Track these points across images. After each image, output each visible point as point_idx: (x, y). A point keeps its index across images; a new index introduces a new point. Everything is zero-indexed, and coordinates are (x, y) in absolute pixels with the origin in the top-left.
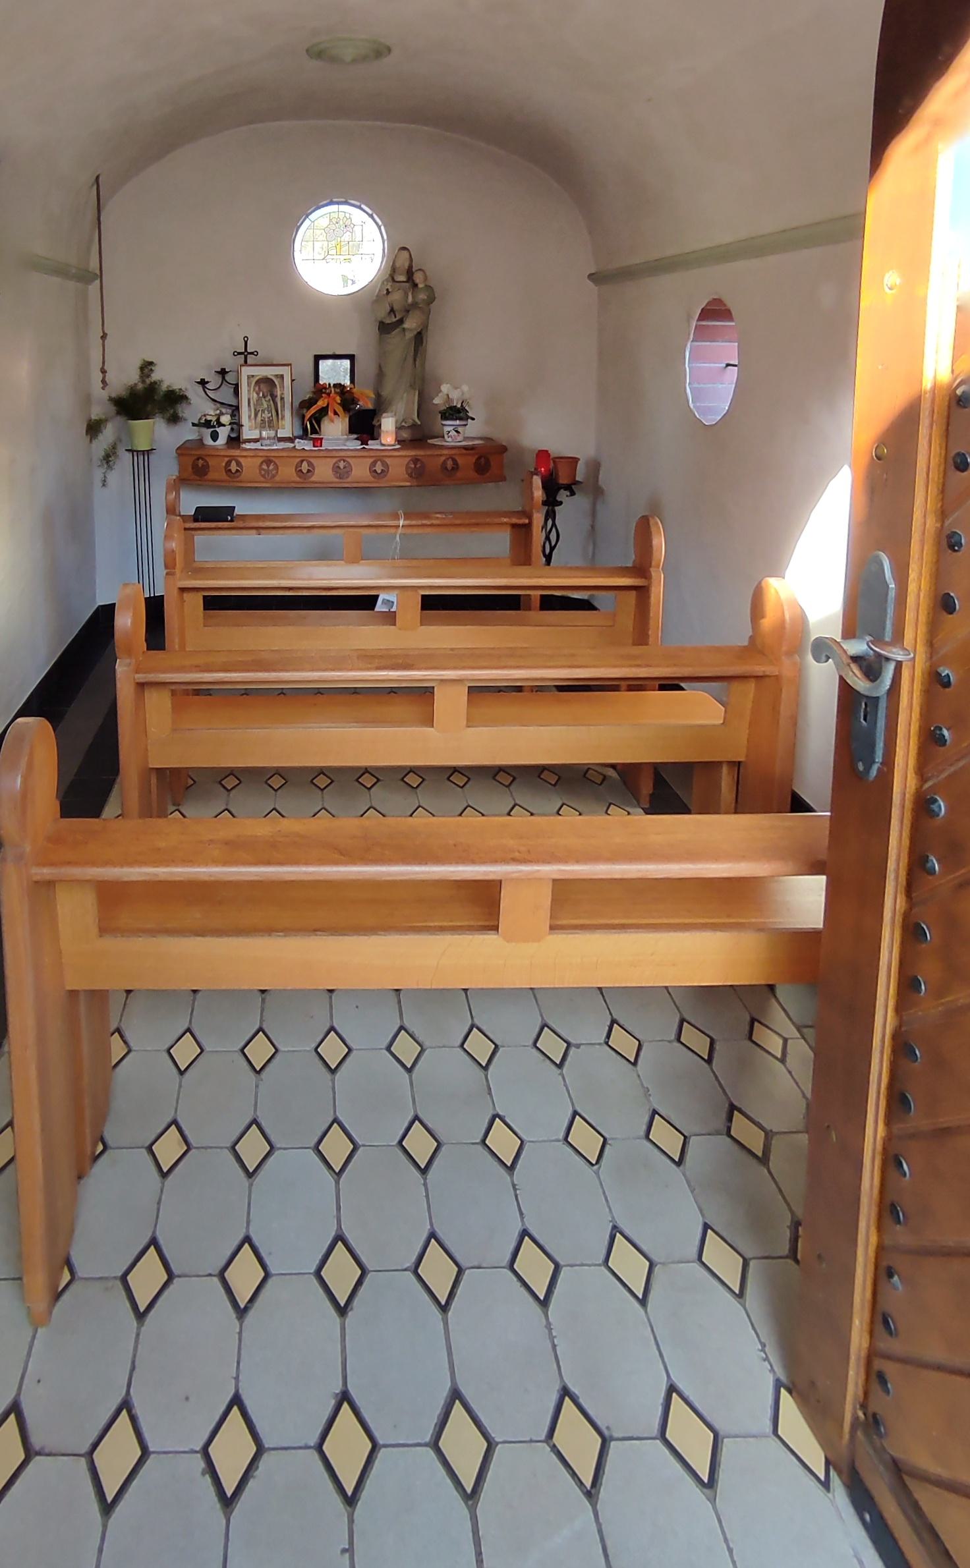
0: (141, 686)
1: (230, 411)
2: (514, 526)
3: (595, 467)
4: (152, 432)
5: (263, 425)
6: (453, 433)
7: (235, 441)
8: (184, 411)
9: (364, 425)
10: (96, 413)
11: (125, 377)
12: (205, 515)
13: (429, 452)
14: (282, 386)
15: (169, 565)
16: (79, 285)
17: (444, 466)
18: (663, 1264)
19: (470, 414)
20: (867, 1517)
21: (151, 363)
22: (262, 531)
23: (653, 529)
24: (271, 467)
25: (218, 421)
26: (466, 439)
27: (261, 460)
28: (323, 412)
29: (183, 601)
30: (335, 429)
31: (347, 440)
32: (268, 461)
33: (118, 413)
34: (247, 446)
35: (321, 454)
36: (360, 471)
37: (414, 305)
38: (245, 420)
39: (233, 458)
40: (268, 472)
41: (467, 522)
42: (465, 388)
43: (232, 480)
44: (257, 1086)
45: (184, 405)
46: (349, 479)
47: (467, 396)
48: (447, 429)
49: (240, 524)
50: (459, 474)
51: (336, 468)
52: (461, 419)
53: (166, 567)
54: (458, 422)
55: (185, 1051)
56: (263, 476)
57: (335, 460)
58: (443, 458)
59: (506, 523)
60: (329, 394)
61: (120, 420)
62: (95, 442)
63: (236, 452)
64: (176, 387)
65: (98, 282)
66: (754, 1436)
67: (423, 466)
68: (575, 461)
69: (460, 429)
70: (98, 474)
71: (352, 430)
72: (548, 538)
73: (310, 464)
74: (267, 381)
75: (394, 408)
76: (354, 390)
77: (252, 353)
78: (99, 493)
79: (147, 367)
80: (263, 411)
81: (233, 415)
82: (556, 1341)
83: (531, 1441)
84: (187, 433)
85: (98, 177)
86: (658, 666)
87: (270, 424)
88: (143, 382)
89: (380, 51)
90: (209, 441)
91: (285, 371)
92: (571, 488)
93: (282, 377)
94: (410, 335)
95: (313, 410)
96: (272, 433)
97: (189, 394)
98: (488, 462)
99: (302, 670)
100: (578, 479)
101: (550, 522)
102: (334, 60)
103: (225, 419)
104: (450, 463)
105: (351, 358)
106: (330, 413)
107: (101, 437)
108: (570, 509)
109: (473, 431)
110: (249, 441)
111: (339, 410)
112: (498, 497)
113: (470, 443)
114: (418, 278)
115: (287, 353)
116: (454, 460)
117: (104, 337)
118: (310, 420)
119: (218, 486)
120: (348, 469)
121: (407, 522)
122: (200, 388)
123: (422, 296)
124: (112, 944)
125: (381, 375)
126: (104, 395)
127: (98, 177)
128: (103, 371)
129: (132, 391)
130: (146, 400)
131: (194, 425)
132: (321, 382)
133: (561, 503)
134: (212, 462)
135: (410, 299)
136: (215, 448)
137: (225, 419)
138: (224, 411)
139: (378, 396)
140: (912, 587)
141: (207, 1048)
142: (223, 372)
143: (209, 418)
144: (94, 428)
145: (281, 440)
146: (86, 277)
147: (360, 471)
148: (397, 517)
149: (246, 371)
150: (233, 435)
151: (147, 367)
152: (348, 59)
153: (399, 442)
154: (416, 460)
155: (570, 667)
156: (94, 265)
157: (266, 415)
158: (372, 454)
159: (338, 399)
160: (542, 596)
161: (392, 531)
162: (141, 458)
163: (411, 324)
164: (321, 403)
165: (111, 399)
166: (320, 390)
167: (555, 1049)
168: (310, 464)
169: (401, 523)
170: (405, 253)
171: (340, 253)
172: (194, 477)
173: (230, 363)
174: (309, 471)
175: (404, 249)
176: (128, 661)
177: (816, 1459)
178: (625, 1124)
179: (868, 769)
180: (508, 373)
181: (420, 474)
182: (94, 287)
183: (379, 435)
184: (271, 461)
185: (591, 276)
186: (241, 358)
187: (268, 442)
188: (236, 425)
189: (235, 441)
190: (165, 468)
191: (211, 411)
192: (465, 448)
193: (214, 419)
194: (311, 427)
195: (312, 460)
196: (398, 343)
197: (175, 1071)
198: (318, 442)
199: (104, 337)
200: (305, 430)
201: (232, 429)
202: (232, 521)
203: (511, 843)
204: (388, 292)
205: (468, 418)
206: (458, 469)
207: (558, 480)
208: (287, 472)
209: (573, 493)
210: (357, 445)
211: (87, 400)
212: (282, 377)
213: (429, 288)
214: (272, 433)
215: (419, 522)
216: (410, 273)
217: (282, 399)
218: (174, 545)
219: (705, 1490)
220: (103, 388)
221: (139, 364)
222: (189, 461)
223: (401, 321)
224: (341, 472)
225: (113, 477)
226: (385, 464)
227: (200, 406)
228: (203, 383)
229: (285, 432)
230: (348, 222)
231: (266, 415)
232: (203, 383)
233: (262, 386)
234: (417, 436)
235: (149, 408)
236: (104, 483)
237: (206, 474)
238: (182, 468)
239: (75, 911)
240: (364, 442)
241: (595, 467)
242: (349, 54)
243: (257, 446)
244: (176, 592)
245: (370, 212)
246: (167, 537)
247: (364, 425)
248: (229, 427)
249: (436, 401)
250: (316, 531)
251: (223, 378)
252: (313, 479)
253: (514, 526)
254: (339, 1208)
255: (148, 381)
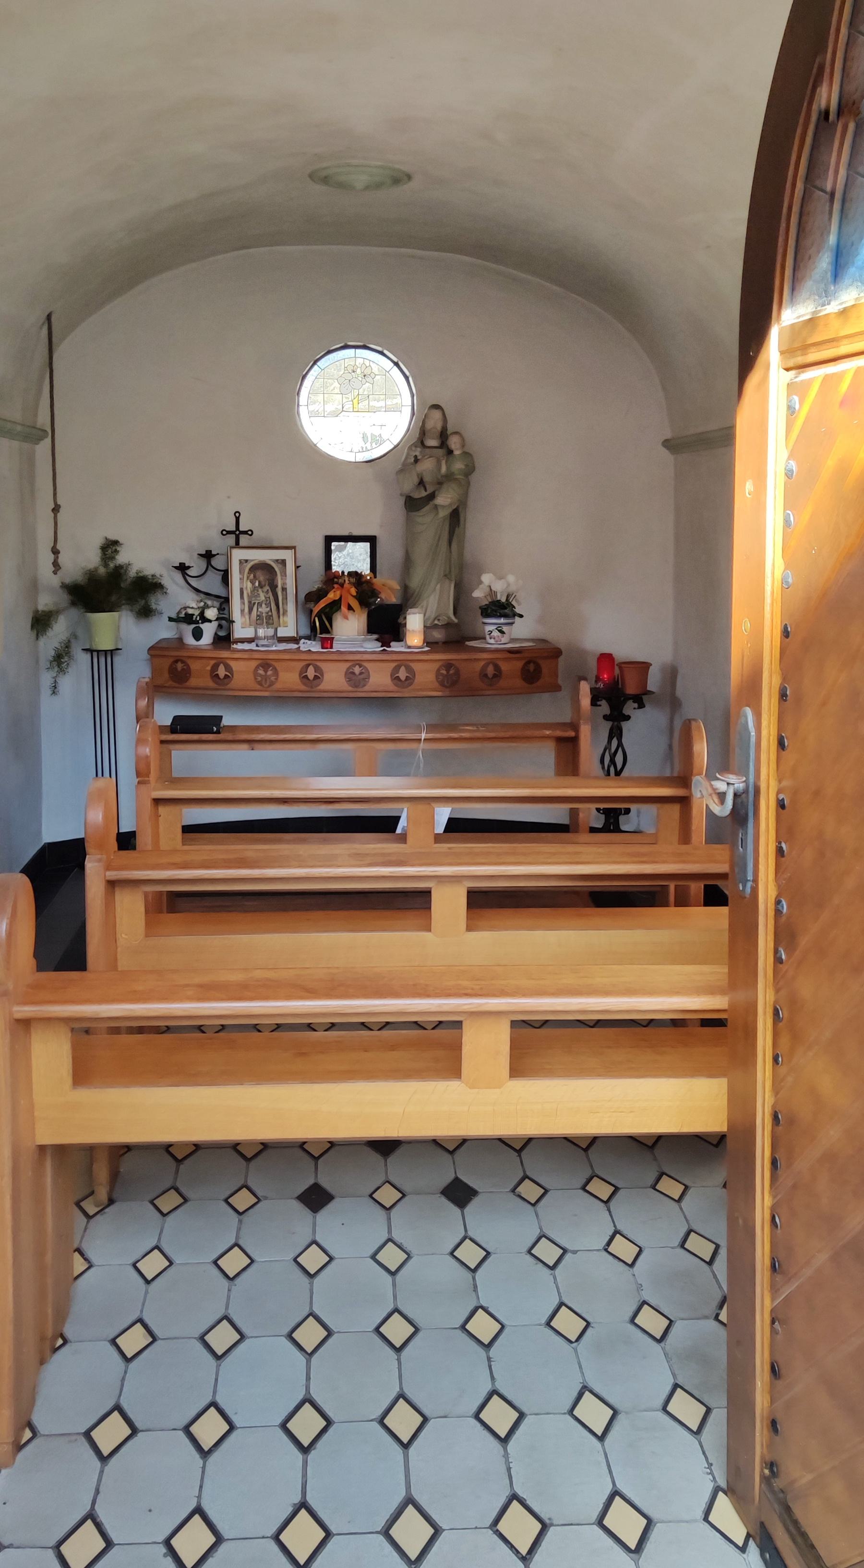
0: (112, 884)
1: (217, 604)
2: (559, 740)
3: (672, 674)
4: (112, 627)
5: (260, 621)
6: (496, 633)
7: (224, 640)
8: (158, 602)
9: (386, 624)
10: (45, 602)
11: (82, 558)
12: (183, 726)
13: (464, 656)
14: (284, 574)
15: (142, 774)
16: (26, 446)
17: (484, 675)
18: (627, 1413)
19: (518, 610)
20: (768, 1556)
21: (116, 543)
22: (256, 745)
23: (695, 733)
24: (270, 673)
25: (202, 614)
26: (513, 640)
27: (254, 664)
28: (335, 606)
29: (158, 816)
30: (350, 628)
31: (364, 640)
32: (265, 665)
33: (73, 604)
34: (240, 646)
35: (335, 657)
36: (379, 679)
37: (449, 477)
38: (236, 615)
39: (219, 661)
40: (266, 678)
41: (502, 734)
42: (511, 578)
43: (220, 685)
44: (229, 1290)
45: (159, 595)
46: (366, 688)
47: (513, 588)
48: (488, 628)
49: (230, 737)
50: (502, 683)
51: (349, 674)
52: (505, 616)
53: (138, 774)
54: (502, 620)
55: (152, 1265)
56: (260, 683)
57: (348, 664)
58: (482, 663)
59: (548, 737)
60: (342, 585)
61: (74, 612)
62: (42, 641)
63: (225, 654)
64: (148, 571)
65: (48, 440)
66: (687, 1522)
67: (457, 673)
68: (644, 667)
69: (505, 629)
70: (46, 678)
71: (371, 629)
72: (613, 761)
73: (317, 669)
74: (264, 567)
75: (424, 603)
76: (374, 580)
77: (245, 533)
78: (48, 705)
79: (110, 547)
80: (260, 604)
81: (221, 609)
82: (511, 1465)
83: (476, 1528)
84: (162, 630)
85: (49, 317)
86: (664, 862)
87: (268, 620)
88: (106, 565)
89: (399, 178)
90: (190, 640)
91: (287, 555)
92: (639, 700)
93: (283, 562)
94: (443, 513)
95: (322, 604)
96: (270, 632)
97: (166, 582)
98: (538, 670)
99: (289, 867)
100: (648, 689)
101: (615, 743)
102: (342, 186)
103: (211, 613)
104: (490, 670)
105: (372, 540)
106: (344, 609)
107: (50, 633)
108: (642, 728)
109: (523, 630)
110: (242, 641)
111: (355, 604)
112: (546, 709)
113: (517, 645)
114: (454, 442)
115: (291, 528)
116: (497, 668)
117: (56, 509)
118: (319, 615)
119: (200, 695)
120: (365, 675)
121: (430, 736)
122: (178, 576)
123: (458, 466)
124: (87, 1095)
125: (408, 563)
126: (55, 581)
127: (49, 317)
128: (55, 552)
129: (92, 576)
130: (110, 588)
131: (171, 619)
132: (335, 568)
133: (628, 718)
134: (195, 666)
135: (444, 469)
136: (197, 649)
137: (211, 613)
138: (209, 603)
139: (406, 588)
140: (764, 733)
141: (177, 1260)
142: (208, 556)
143: (190, 611)
144: (41, 622)
145: (282, 640)
146: (32, 435)
147: (379, 679)
148: (419, 729)
149: (238, 555)
150: (222, 633)
151: (110, 547)
152: (359, 186)
153: (427, 642)
154: (448, 665)
155: (571, 863)
156: (43, 419)
157: (264, 609)
158: (395, 657)
159: (353, 591)
160: (571, 809)
161: (413, 745)
162: (102, 660)
163: (445, 499)
164: (332, 596)
165: (65, 586)
166: (331, 579)
167: (549, 1253)
168: (317, 669)
169: (423, 736)
170: (437, 414)
171: (356, 410)
172: (170, 683)
173: (218, 544)
174: (316, 677)
175: (436, 407)
176: (99, 856)
177: (738, 1533)
178: (608, 1315)
179: (744, 886)
180: (548, 559)
181: (453, 682)
182: (43, 448)
183: (404, 635)
184: (269, 665)
185: (667, 444)
186: (231, 539)
187: (265, 642)
188: (225, 620)
189: (224, 640)
190: (133, 672)
191: (192, 603)
192: (510, 651)
193: (197, 612)
194: (321, 626)
195: (319, 664)
196: (429, 524)
197: (141, 1281)
198: (327, 643)
199: (56, 509)
200: (313, 628)
201: (220, 626)
202: (218, 732)
203: (465, 983)
204: (416, 460)
205: (515, 615)
206: (501, 677)
207: (619, 691)
208: (289, 678)
209: (641, 706)
210: (372, 645)
211: (33, 587)
212: (283, 562)
213: (467, 455)
214: (270, 632)
215: (445, 735)
216: (444, 436)
217: (284, 589)
218: (146, 750)
219: (631, 1555)
220: (55, 573)
221: (99, 542)
222: (166, 663)
223: (432, 496)
224: (356, 678)
225: (66, 683)
226: (409, 670)
227: (178, 596)
228: (182, 568)
229: (288, 629)
230: (367, 371)
231: (264, 609)
232: (182, 568)
233: (259, 573)
234: (452, 637)
235: (114, 598)
236: (54, 689)
237: (187, 679)
238: (155, 671)
239: (51, 1055)
240: (385, 643)
241: (672, 674)
242: (360, 180)
243: (253, 646)
244: (148, 804)
245: (395, 360)
246: (140, 741)
247: (386, 624)
248: (215, 625)
249: (478, 594)
250: (322, 746)
251: (209, 564)
252: (321, 687)
253: (559, 740)
254: (308, 1378)
255: (112, 565)
